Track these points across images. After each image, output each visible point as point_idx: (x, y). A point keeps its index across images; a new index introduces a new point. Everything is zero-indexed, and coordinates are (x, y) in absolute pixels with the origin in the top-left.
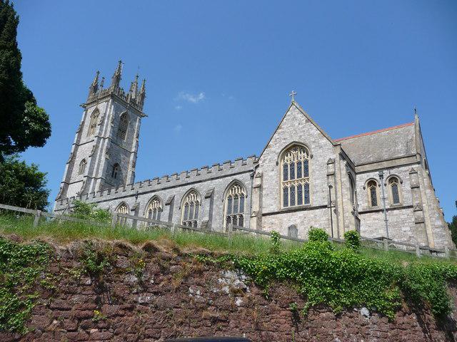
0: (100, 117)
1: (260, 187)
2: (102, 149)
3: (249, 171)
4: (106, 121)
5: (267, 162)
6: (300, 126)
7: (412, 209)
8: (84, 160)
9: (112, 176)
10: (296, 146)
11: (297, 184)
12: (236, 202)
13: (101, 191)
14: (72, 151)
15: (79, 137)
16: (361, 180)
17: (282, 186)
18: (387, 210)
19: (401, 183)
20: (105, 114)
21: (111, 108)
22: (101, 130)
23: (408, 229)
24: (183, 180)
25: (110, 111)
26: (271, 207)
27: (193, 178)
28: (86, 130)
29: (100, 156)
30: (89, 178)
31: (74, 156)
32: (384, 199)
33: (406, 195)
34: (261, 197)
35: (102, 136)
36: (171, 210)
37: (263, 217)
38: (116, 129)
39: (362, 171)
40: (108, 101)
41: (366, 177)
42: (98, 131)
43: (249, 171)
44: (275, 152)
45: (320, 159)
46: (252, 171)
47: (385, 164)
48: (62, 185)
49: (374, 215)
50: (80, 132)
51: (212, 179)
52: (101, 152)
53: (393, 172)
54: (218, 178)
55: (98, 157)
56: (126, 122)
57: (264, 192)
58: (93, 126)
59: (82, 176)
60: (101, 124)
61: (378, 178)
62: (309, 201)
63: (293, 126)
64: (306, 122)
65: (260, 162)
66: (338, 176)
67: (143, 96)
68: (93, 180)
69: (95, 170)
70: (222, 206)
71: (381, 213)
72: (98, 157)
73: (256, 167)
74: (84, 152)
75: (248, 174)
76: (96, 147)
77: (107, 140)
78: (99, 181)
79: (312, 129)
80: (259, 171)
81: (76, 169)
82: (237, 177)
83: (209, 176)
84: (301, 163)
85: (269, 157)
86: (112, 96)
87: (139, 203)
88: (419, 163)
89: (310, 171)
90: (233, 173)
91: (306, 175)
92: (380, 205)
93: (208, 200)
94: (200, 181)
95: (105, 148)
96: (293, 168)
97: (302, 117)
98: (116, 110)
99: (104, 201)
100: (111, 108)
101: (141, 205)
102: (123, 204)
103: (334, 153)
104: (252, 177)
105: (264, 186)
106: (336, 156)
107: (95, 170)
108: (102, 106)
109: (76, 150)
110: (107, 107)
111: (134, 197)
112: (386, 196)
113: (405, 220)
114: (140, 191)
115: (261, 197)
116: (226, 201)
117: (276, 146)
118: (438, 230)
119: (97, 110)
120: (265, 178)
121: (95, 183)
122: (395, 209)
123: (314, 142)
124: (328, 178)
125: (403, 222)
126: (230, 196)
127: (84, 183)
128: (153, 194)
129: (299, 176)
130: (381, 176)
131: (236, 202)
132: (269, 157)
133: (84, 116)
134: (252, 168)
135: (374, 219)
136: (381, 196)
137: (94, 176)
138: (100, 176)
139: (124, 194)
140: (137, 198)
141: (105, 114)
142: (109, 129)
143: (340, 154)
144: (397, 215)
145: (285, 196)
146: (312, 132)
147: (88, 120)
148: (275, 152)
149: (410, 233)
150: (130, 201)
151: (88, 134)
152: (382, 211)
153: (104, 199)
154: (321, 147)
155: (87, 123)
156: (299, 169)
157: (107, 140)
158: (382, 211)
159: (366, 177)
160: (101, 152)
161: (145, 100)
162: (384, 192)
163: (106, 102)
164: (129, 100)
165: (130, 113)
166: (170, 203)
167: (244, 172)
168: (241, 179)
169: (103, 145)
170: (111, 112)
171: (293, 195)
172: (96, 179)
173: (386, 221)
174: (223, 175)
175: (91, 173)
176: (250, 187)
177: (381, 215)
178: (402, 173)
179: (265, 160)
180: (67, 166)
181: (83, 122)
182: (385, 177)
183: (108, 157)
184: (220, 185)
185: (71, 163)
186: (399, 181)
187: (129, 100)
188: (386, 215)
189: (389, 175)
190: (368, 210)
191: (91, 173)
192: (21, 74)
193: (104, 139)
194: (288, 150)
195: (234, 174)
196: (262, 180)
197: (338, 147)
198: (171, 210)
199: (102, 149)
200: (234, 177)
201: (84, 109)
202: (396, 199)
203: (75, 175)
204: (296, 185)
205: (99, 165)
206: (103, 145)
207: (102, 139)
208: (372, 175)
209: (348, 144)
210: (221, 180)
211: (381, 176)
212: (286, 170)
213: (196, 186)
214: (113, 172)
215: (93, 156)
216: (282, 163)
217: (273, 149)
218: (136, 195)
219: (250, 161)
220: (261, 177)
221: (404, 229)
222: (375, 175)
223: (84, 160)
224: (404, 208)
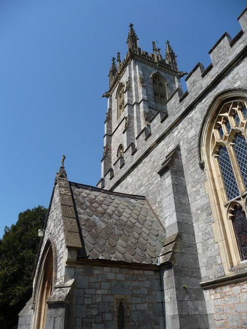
2: (138, 118)
13: (149, 118)
14: (105, 145)
15: (110, 126)
21: (135, 69)
22: (130, 96)
25: (135, 72)
28: (114, 115)
31: (108, 149)
50: (109, 119)
56: (161, 85)
77: (142, 105)
95: (142, 114)
100: (135, 69)
109: (109, 142)
121: (138, 108)
133: (108, 103)
138: (141, 97)
161: (177, 59)
165: (162, 74)
169: (138, 113)
181: (110, 109)
185: (106, 157)
192: (20, 215)
193: (138, 104)
199: (138, 118)
206: (138, 113)
207: (135, 107)
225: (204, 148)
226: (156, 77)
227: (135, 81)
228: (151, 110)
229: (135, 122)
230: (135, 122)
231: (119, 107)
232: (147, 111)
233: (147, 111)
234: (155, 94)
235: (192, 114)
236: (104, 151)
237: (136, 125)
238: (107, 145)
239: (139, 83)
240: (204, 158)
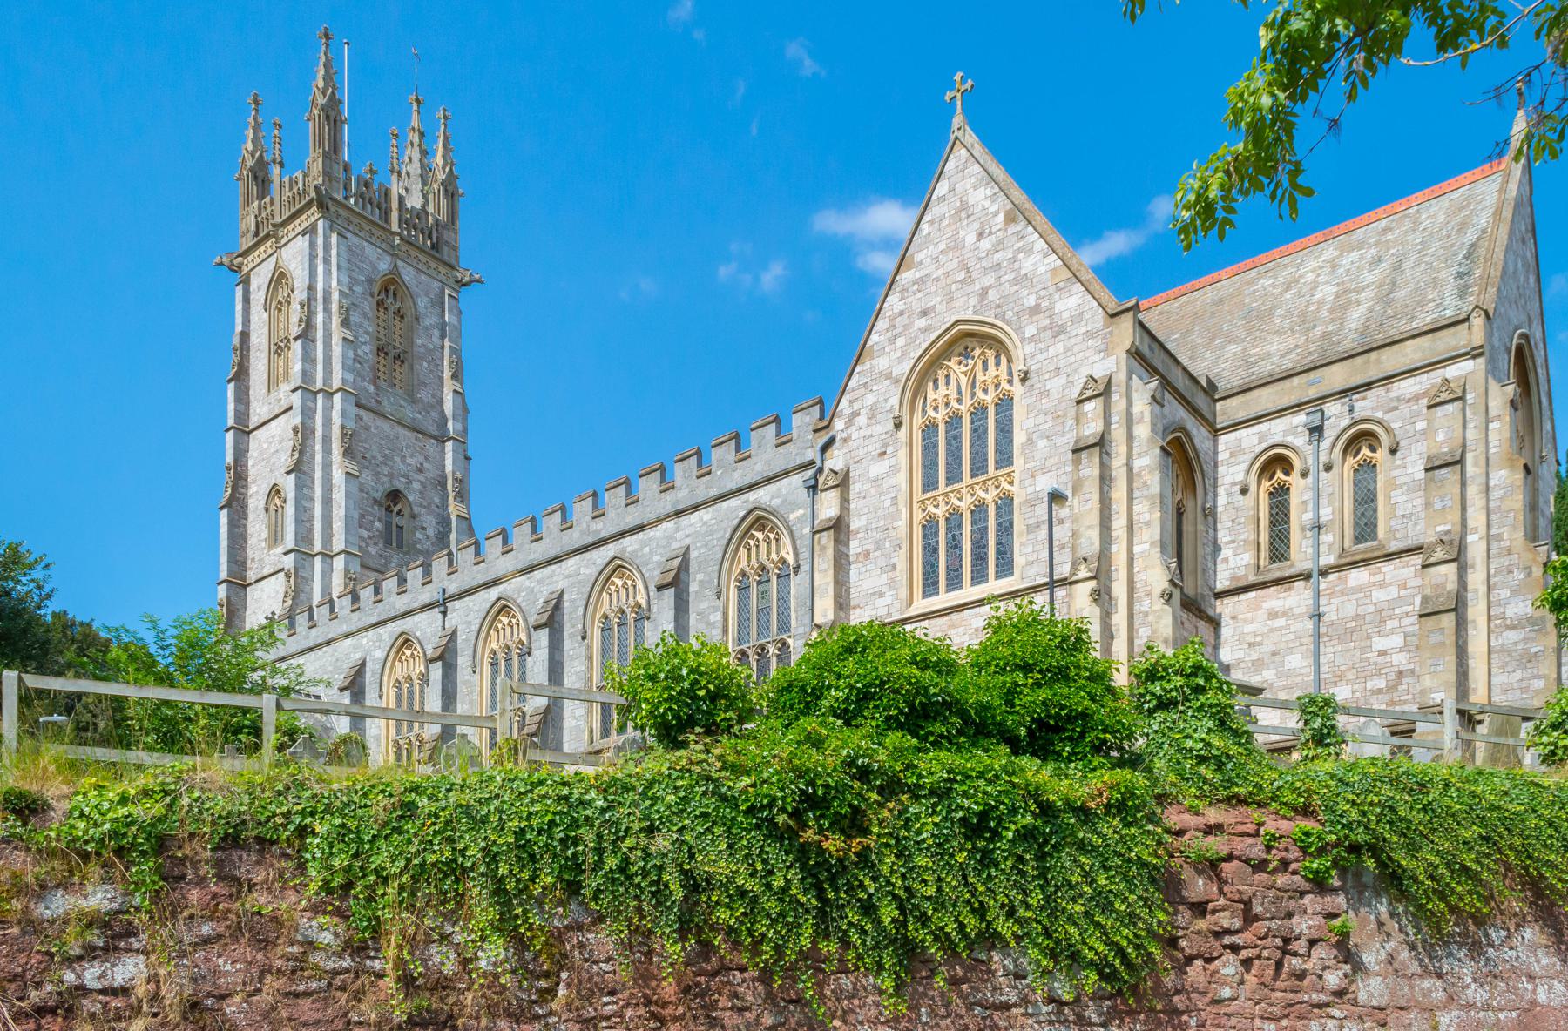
0: (295, 306)
1: (838, 527)
2: (327, 440)
3: (802, 467)
4: (320, 318)
5: (862, 420)
6: (986, 244)
7: (1417, 560)
8: (275, 491)
9: (388, 543)
10: (966, 340)
11: (968, 500)
12: (763, 595)
15: (243, 398)
16: (1233, 458)
17: (918, 516)
18: (1324, 573)
19: (1393, 451)
20: (311, 288)
22: (308, 358)
23: (1396, 641)
24: (585, 526)
25: (327, 273)
26: (880, 602)
27: (618, 515)
29: (327, 466)
30: (303, 553)
31: (240, 477)
32: (1318, 527)
33: (1405, 507)
34: (841, 564)
35: (319, 385)
36: (555, 646)
37: (1218, 602)
38: (367, 350)
39: (1241, 416)
40: (311, 230)
41: (1251, 441)
42: (297, 367)
43: (802, 467)
44: (889, 376)
45: (1055, 385)
46: (812, 463)
47: (1337, 377)
48: (222, 592)
49: (1273, 599)
50: (241, 375)
51: (680, 513)
52: (327, 451)
53: (1366, 405)
54: (695, 508)
55: (318, 474)
57: (855, 547)
58: (279, 348)
59: (279, 550)
60: (306, 335)
61: (1300, 440)
62: (1373, 526)
63: (956, 245)
64: (1010, 219)
65: (838, 425)
66: (1119, 449)
67: (450, 190)
68: (318, 559)
69: (318, 526)
70: (716, 617)
71: (1299, 585)
72: (318, 474)
73: (825, 448)
74: (269, 453)
75: (797, 480)
76: (304, 433)
78: (339, 563)
79: (1028, 251)
80: (836, 460)
81: (257, 527)
82: (762, 496)
83: (669, 502)
84: (984, 408)
85: (870, 399)
86: (322, 202)
87: (454, 634)
88: (1475, 353)
89: (1019, 438)
90: (748, 481)
91: (1005, 459)
92: (1301, 553)
93: (670, 593)
94: (640, 528)
96: (957, 438)
97: (993, 198)
98: (352, 261)
99: (347, 636)
101: (461, 637)
102: (405, 641)
103: (1107, 351)
104: (813, 488)
105: (856, 523)
106: (1112, 364)
107: (318, 526)
108: (294, 255)
109: (241, 453)
110: (313, 258)
111: (435, 614)
112: (1326, 513)
113: (1391, 604)
114: (452, 589)
115: (841, 564)
116: (733, 594)
117: (892, 352)
118: (1512, 636)
119: (279, 278)
120: (856, 488)
122: (1354, 564)
123: (1035, 310)
124: (1077, 463)
125: (1382, 615)
126: (743, 574)
127: (288, 576)
128: (493, 593)
129: (979, 468)
130: (1317, 431)
131: (763, 595)
132: (870, 399)
133: (239, 307)
134: (810, 454)
135: (1273, 615)
136: (1308, 516)
137: (318, 547)
139: (401, 604)
140: (444, 613)
141: (311, 288)
142: (337, 349)
143: (1135, 354)
144: (1359, 589)
145: (930, 550)
146: (1027, 264)
147: (259, 317)
148: (889, 376)
149: (1400, 660)
150: (427, 628)
151: (272, 383)
152: (1307, 576)
153: (345, 629)
154: (1059, 331)
155: (259, 338)
156: (979, 434)
157: (338, 398)
158: (1307, 576)
159: (1251, 441)
160: (327, 451)
161: (461, 203)
162: (1321, 499)
163: (303, 233)
164: (395, 216)
166: (552, 620)
167: (785, 474)
168: (776, 502)
169: (328, 422)
170: (332, 281)
171: (954, 545)
172: (328, 557)
173: (1317, 616)
174: (714, 492)
175: (304, 536)
176: (807, 530)
177: (1298, 597)
178: (1395, 405)
179: (856, 414)
180: (224, 516)
181: (245, 335)
182: (1330, 434)
183: (354, 469)
184: (704, 531)
185: (236, 505)
186: (1385, 440)
187: (395, 216)
188: (1318, 594)
189: (1346, 422)
190: (1252, 579)
191: (304, 536)
194: (929, 369)
195: (753, 486)
196: (845, 501)
197: (1127, 322)
198: (555, 646)
199: (327, 440)
200: (752, 497)
201: (237, 277)
202: (1365, 528)
203: (264, 555)
204: (965, 505)
205: (327, 502)
208: (1277, 430)
209: (1170, 316)
210: (705, 515)
211: (1317, 431)
212: (929, 449)
213: (629, 543)
214: (388, 525)
215: (299, 468)
216: (918, 420)
217: (882, 363)
218: (442, 604)
219: (802, 423)
220: (843, 482)
221: (1379, 643)
222: (1288, 431)
223: (275, 491)
224: (1389, 556)
225: (385, 678)
226: (390, 288)
227: (327, 310)
228: (362, 413)
229: (318, 447)
230: (318, 447)
231: (273, 348)
232: (351, 425)
233: (351, 425)
234: (380, 350)
235: (381, 630)
236: (228, 477)
237: (319, 458)
238: (236, 461)
239: (336, 321)
240: (384, 689)
